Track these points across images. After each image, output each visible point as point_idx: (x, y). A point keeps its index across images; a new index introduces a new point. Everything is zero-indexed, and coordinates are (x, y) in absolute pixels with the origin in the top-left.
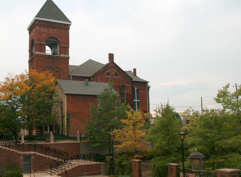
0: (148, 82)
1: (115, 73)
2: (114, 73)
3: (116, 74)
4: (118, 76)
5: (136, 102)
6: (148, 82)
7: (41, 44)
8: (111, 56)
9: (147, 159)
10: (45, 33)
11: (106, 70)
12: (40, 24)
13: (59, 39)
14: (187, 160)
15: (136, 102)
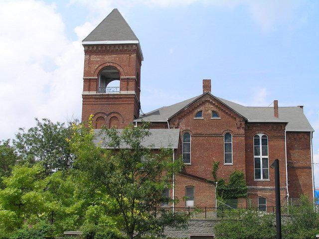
0: (286, 124)
1: (213, 111)
2: (210, 112)
3: (215, 114)
4: (218, 117)
5: (261, 159)
6: (286, 124)
7: (90, 79)
8: (207, 84)
9: (36, 184)
10: (97, 62)
11: (196, 108)
12: (100, 51)
13: (119, 68)
14: (66, 185)
15: (261, 159)
